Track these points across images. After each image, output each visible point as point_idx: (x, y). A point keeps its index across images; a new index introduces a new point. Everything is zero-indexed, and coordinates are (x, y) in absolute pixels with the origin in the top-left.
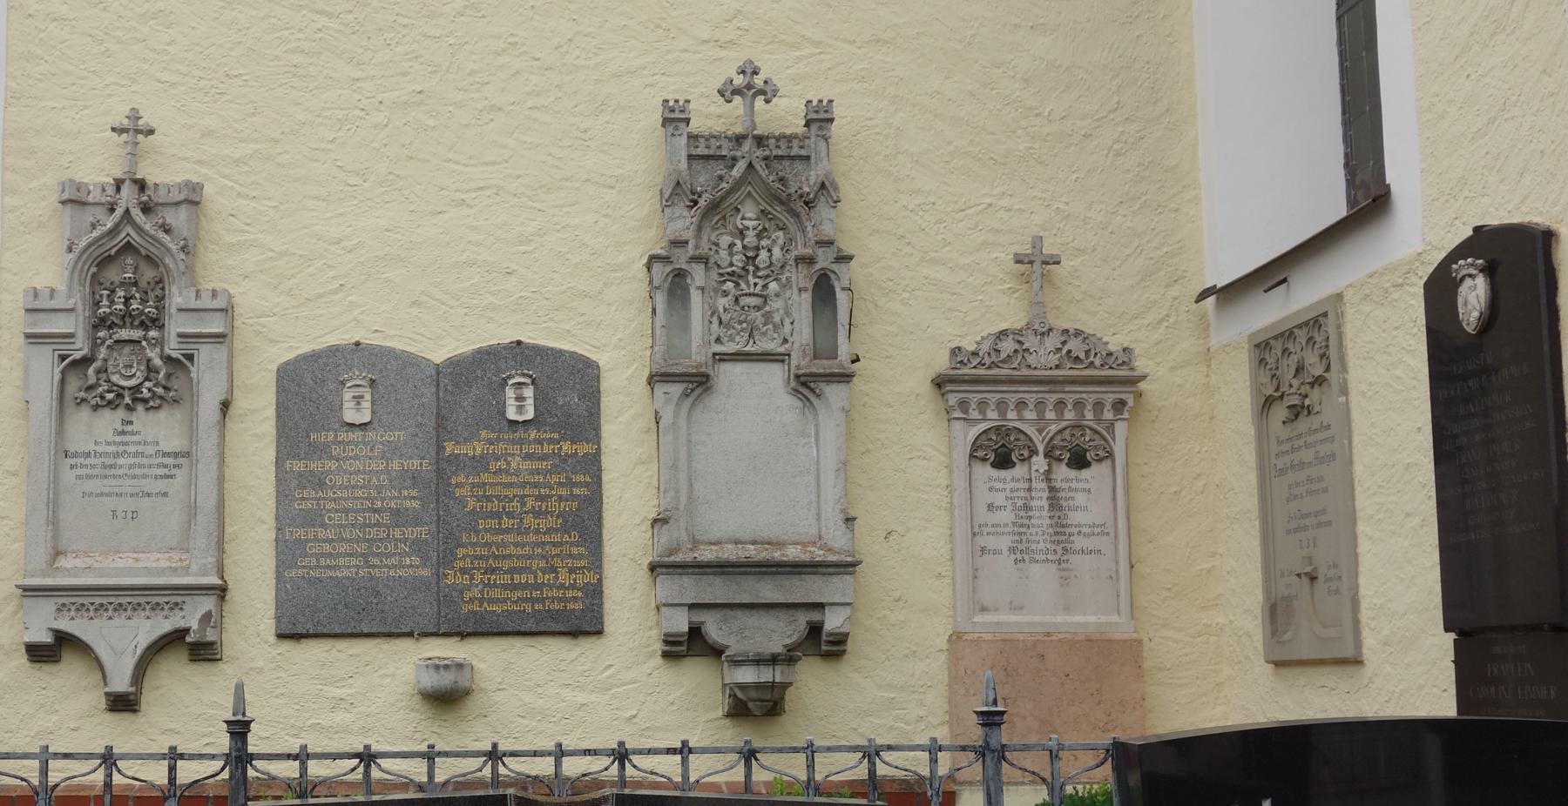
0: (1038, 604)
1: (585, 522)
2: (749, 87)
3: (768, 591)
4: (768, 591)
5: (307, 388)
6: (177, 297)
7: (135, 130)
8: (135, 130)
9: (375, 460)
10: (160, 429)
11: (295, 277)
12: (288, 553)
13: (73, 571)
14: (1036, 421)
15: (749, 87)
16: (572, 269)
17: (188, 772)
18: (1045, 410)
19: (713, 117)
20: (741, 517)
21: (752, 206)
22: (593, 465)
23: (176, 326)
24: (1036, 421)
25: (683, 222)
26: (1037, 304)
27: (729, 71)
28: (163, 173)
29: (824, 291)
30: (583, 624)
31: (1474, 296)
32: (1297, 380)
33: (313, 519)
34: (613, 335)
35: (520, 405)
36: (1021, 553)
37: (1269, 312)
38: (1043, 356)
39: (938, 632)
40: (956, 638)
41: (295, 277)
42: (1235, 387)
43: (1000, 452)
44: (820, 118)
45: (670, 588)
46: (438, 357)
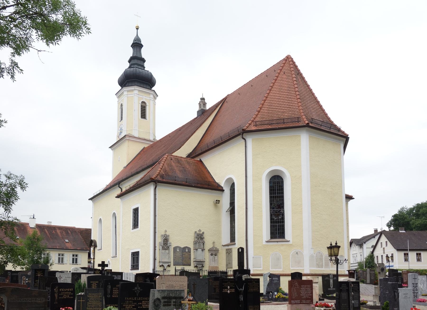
0: (213, 265)
1: (190, 258)
2: (200, 231)
3: (200, 263)
4: (200, 263)
5: (175, 249)
6: (168, 243)
7: (166, 231)
8: (166, 231)
9: (179, 254)
10: (167, 251)
11: (174, 242)
12: (174, 260)
13: (163, 261)
14: (214, 253)
15: (200, 231)
16: (187, 241)
17: (58, 279)
18: (214, 252)
19: (198, 232)
20: (199, 258)
21: (200, 238)
22: (190, 255)
23: (168, 245)
24: (214, 253)
25: (196, 239)
26: (214, 245)
27: (199, 230)
28: (167, 234)
29: (203, 244)
30: (190, 265)
31: (240, 250)
32: (229, 252)
33: (175, 258)
34: (191, 246)
35: (187, 251)
36: (213, 261)
37: (227, 248)
38: (214, 249)
39: (208, 266)
40: (209, 266)
41: (174, 242)
42: (224, 252)
43: (212, 255)
44: (203, 233)
45: (195, 263)
46: (182, 247)
